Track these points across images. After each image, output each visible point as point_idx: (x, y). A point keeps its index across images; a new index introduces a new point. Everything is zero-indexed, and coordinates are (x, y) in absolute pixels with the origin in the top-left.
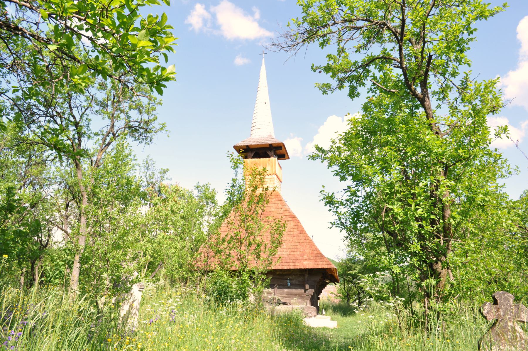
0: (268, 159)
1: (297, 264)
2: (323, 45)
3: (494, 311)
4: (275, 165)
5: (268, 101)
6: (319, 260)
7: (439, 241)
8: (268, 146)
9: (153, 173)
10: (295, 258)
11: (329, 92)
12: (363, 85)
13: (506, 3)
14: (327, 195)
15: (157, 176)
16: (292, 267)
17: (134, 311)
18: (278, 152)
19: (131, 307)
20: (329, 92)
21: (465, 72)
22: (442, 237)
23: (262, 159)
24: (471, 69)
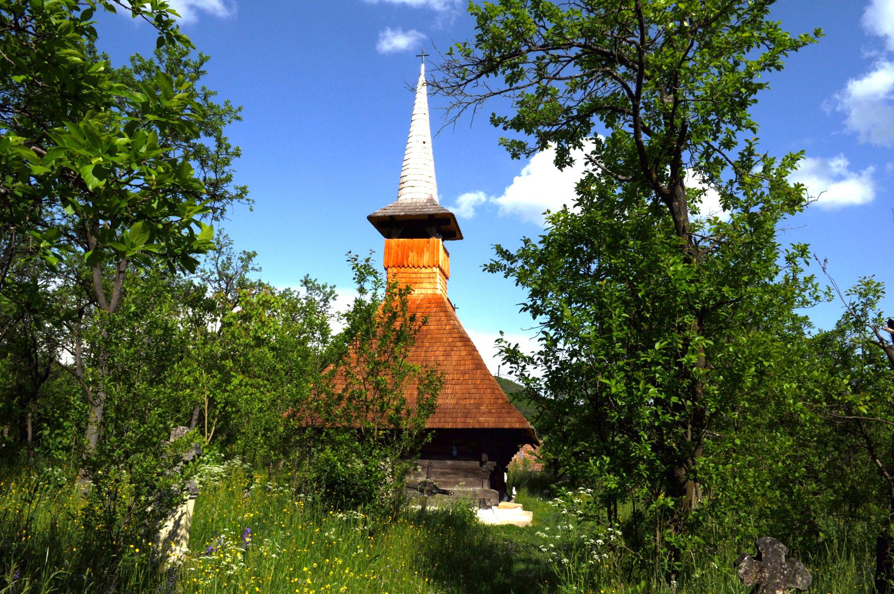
0: (426, 240)
1: (468, 420)
3: (755, 569)
4: (438, 250)
5: (429, 139)
6: (505, 415)
7: (686, 433)
9: (229, 259)
10: (465, 411)
11: (523, 156)
12: (580, 148)
13: (820, 30)
14: (506, 346)
15: (236, 263)
16: (460, 426)
17: (182, 532)
18: (443, 227)
19: (177, 524)
20: (523, 156)
21: (747, 140)
24: (757, 136)
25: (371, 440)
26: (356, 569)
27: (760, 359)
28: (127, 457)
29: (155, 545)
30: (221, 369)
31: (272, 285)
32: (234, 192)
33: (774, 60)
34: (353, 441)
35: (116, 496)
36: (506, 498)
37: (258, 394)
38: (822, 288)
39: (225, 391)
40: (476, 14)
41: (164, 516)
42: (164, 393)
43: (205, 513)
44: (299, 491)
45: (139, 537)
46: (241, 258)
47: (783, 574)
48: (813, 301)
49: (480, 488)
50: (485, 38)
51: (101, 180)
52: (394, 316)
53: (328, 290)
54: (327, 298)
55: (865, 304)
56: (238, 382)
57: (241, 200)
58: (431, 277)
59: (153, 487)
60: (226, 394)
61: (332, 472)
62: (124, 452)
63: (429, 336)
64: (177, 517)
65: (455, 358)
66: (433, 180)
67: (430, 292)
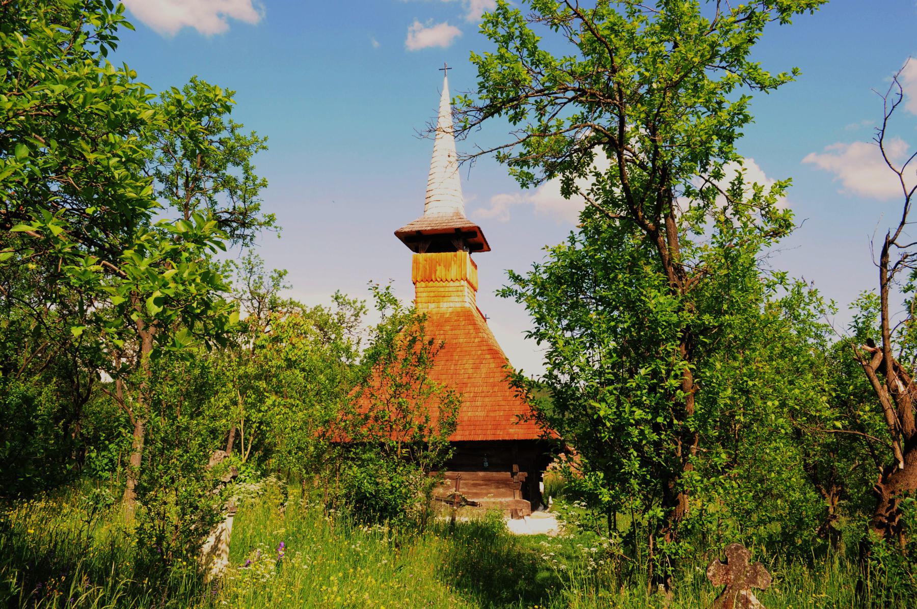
0: (453, 253)
1: (498, 432)
2: (515, 119)
3: (722, 572)
4: (465, 263)
7: (676, 449)
8: (454, 232)
9: (260, 278)
11: (531, 186)
12: (584, 177)
15: (268, 282)
16: (490, 438)
17: (223, 546)
18: (471, 240)
19: (218, 539)
20: (531, 186)
21: (736, 171)
23: (443, 254)
24: (744, 166)
25: (395, 457)
27: (745, 378)
28: (173, 482)
29: (199, 559)
30: (256, 390)
31: (302, 302)
32: (262, 220)
33: (742, 110)
35: (164, 516)
36: (541, 507)
37: (291, 414)
38: (826, 302)
39: (260, 411)
41: (207, 533)
42: (204, 425)
43: (244, 530)
45: (185, 552)
46: (272, 277)
47: (746, 576)
48: (818, 314)
49: (513, 498)
50: (487, 85)
51: (159, 307)
52: (414, 341)
53: (358, 305)
54: (358, 313)
57: (269, 228)
58: (459, 290)
59: (196, 508)
60: (260, 415)
62: (170, 478)
63: (458, 350)
64: (218, 533)
65: (484, 370)
67: (458, 305)
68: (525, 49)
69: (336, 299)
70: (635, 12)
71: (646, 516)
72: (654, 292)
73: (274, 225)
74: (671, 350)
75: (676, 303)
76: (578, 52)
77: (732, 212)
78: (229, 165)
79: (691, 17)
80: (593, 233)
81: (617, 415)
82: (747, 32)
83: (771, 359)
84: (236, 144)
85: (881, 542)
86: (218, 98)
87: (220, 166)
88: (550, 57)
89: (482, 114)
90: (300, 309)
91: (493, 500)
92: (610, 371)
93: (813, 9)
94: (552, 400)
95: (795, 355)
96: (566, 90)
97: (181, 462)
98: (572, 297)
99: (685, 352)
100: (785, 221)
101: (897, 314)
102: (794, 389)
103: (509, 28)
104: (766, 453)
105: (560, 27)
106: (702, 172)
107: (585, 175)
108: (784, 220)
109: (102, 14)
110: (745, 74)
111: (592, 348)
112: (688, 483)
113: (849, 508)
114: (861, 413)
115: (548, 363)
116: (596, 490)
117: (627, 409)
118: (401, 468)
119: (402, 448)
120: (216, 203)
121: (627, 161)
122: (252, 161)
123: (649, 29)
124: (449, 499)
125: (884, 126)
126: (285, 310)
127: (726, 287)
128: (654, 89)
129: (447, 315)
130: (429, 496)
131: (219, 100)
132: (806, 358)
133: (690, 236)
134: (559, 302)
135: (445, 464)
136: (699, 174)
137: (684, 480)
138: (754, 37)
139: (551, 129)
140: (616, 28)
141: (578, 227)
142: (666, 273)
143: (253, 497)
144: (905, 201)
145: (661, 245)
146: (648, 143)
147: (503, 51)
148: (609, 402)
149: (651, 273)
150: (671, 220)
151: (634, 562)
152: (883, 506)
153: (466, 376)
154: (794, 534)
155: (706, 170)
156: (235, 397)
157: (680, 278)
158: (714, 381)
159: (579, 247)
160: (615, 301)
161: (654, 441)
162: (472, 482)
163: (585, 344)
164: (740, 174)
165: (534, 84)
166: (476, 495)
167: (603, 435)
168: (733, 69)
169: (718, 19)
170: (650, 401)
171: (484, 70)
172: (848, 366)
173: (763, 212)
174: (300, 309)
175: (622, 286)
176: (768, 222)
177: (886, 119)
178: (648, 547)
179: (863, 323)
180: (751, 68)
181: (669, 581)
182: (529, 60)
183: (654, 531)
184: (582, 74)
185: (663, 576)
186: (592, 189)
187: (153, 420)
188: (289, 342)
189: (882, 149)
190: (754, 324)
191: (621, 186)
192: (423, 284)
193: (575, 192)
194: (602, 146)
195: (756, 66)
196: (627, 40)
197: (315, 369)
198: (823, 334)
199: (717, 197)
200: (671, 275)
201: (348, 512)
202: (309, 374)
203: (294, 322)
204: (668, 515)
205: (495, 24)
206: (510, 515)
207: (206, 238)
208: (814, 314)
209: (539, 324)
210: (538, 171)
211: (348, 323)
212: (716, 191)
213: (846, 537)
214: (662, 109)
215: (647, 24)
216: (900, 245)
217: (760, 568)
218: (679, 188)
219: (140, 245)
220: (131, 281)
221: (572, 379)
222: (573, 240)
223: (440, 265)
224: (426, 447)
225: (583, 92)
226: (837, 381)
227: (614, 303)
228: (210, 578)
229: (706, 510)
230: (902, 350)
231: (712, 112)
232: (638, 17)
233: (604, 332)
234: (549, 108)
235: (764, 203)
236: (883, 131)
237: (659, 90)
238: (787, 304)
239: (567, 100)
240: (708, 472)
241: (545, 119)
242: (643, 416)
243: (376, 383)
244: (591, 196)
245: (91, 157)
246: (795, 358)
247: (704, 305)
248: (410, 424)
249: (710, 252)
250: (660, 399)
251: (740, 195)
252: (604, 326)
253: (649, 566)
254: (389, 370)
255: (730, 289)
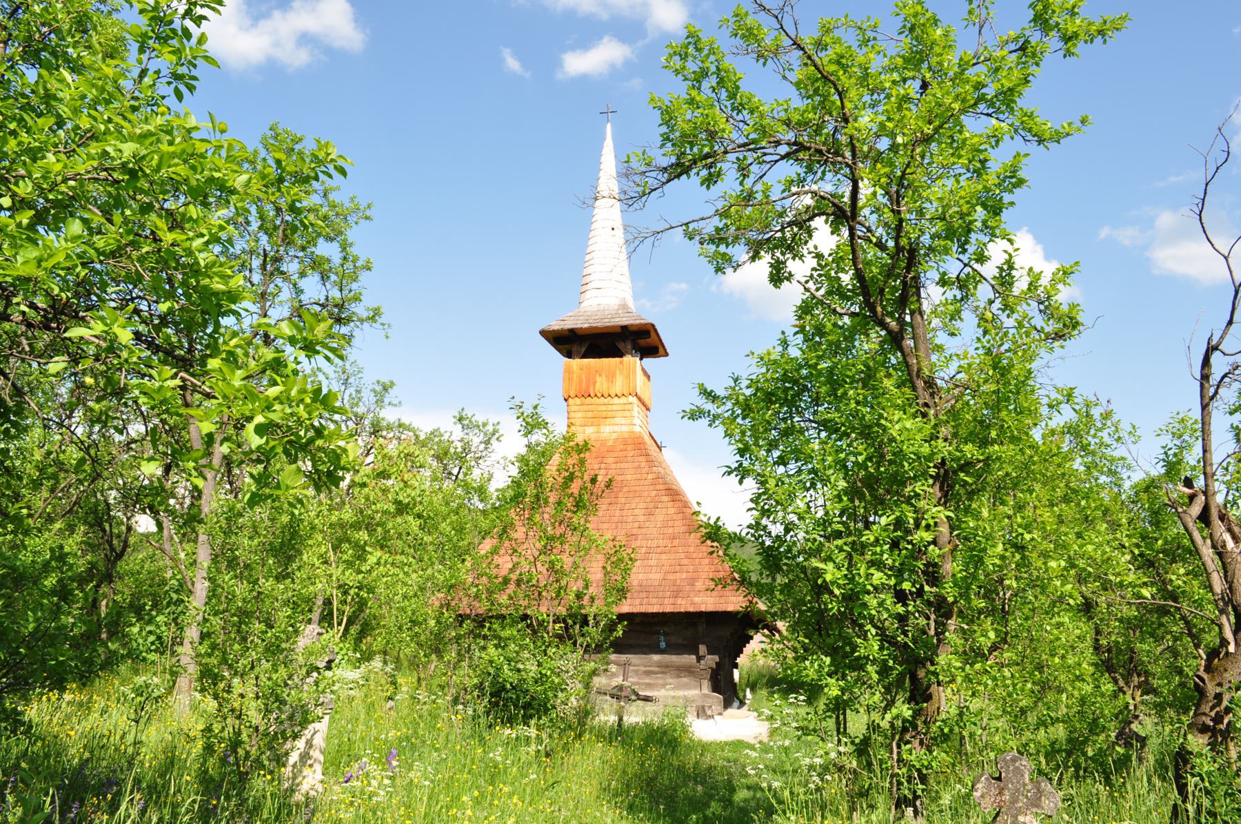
0: (618, 359)
1: (679, 601)
2: (710, 181)
3: (994, 791)
4: (635, 373)
7: (928, 624)
8: (620, 330)
9: (358, 392)
11: (729, 271)
12: (800, 259)
16: (668, 609)
17: (315, 754)
18: (642, 342)
19: (309, 744)
20: (729, 271)
21: (1006, 252)
22: (933, 617)
23: (604, 360)
24: (1016, 246)
25: (545, 635)
26: (528, 799)
27: (1020, 530)
28: (252, 668)
31: (415, 425)
32: (364, 314)
33: (1015, 171)
34: (523, 638)
35: (240, 715)
36: (736, 704)
37: (401, 576)
38: (1125, 427)
39: (359, 572)
40: (660, 108)
41: (296, 736)
42: (294, 590)
44: (456, 701)
46: (374, 391)
47: (1027, 797)
48: (1114, 443)
49: (701, 691)
50: (671, 136)
51: (262, 438)
52: (571, 478)
53: (490, 428)
54: (490, 439)
55: (1181, 448)
56: (375, 560)
57: (374, 324)
58: (627, 409)
60: (360, 576)
61: (496, 676)
63: (625, 489)
64: (309, 737)
66: (626, 279)
67: (625, 429)
68: (724, 90)
69: (459, 420)
70: (869, 41)
71: (888, 717)
72: (898, 415)
73: (380, 320)
74: (921, 493)
75: (928, 429)
76: (793, 93)
77: (1000, 306)
78: (321, 241)
79: (944, 47)
80: (814, 335)
81: (849, 579)
82: (1019, 67)
83: (1052, 505)
84: (331, 213)
85: (1204, 752)
86: (330, 157)
87: (308, 242)
88: (756, 99)
89: (666, 175)
90: (411, 434)
91: (672, 693)
92: (839, 519)
93: (1107, 38)
94: (759, 558)
95: (1083, 498)
96: (778, 143)
97: (263, 640)
98: (784, 420)
99: (939, 495)
100: (1071, 318)
101: (1223, 444)
102: (1085, 545)
103: (702, 62)
104: (1046, 631)
105: (770, 60)
106: (960, 253)
107: (801, 257)
108: (1070, 318)
109: (178, 46)
110: (1017, 123)
111: (815, 489)
112: (944, 671)
113: (1156, 705)
114: (1174, 577)
115: (754, 509)
116: (821, 680)
117: (862, 572)
118: (554, 650)
119: (554, 622)
120: (302, 291)
121: (859, 237)
122: (351, 235)
123: (888, 63)
124: (615, 691)
125: (1205, 193)
126: (391, 435)
127: (996, 407)
128: (899, 145)
129: (610, 443)
130: (587, 686)
131: (332, 160)
132: (1099, 503)
133: (941, 338)
134: (768, 426)
135: (613, 644)
136: (956, 256)
137: (939, 667)
138: (1028, 75)
139: (756, 195)
140: (844, 61)
141: (794, 326)
142: (914, 388)
143: (351, 689)
144: (1233, 293)
145: (907, 351)
146: (888, 216)
147: (694, 93)
148: (837, 561)
149: (892, 388)
150: (919, 317)
151: (871, 778)
152: (1207, 702)
153: (636, 525)
154: (1085, 742)
155: (964, 251)
156: (326, 552)
157: (932, 395)
158: (980, 533)
159: (794, 352)
160: (845, 426)
161: (899, 614)
162: (644, 669)
163: (805, 483)
164: (1010, 255)
165: (734, 136)
166: (649, 686)
167: (830, 606)
168: (1001, 116)
169: (981, 51)
170: (894, 560)
171: (668, 117)
172: (1155, 513)
173: (1042, 307)
174: (411, 434)
175: (853, 405)
176: (1049, 319)
177: (1207, 184)
178: (891, 758)
179: (1175, 455)
180: (1025, 115)
181: (918, 803)
182: (728, 104)
183: (897, 737)
184: (799, 123)
185: (911, 797)
186: (812, 275)
187: (227, 583)
188: (399, 478)
189: (1202, 224)
190: (1031, 457)
191: (852, 272)
192: (578, 401)
193: (788, 279)
194: (824, 217)
195: (1032, 113)
196: (860, 77)
197: (436, 515)
198: (1119, 470)
199: (980, 286)
200: (920, 391)
201: (481, 709)
202: (428, 522)
203: (406, 451)
204: (917, 713)
205: (684, 57)
206: (695, 714)
207: (318, 344)
208: (1109, 443)
209: (742, 456)
210: (740, 252)
211: (475, 453)
212: (978, 278)
213: (1153, 743)
214: (908, 171)
215: (885, 56)
216: (1227, 352)
217: (1046, 785)
218: (930, 275)
219: (230, 353)
220: (221, 400)
221: (787, 530)
222: (785, 343)
223: (600, 375)
224: (585, 622)
225: (801, 147)
226: (1141, 534)
227: (843, 428)
228: (298, 797)
229: (968, 708)
230: (1228, 492)
231: (973, 173)
232: (873, 47)
233: (830, 467)
234: (755, 168)
235: (1042, 295)
236: (1203, 200)
237: (905, 145)
238: (1072, 430)
239: (778, 157)
240: (974, 655)
241: (748, 183)
242: (883, 581)
243: (519, 533)
244: (811, 285)
245: (168, 237)
246: (1083, 503)
247: (963, 432)
248: (565, 591)
249: (970, 360)
250: (906, 557)
251: (1011, 284)
252: (830, 459)
253: (891, 783)
254: (537, 518)
255: (999, 411)
